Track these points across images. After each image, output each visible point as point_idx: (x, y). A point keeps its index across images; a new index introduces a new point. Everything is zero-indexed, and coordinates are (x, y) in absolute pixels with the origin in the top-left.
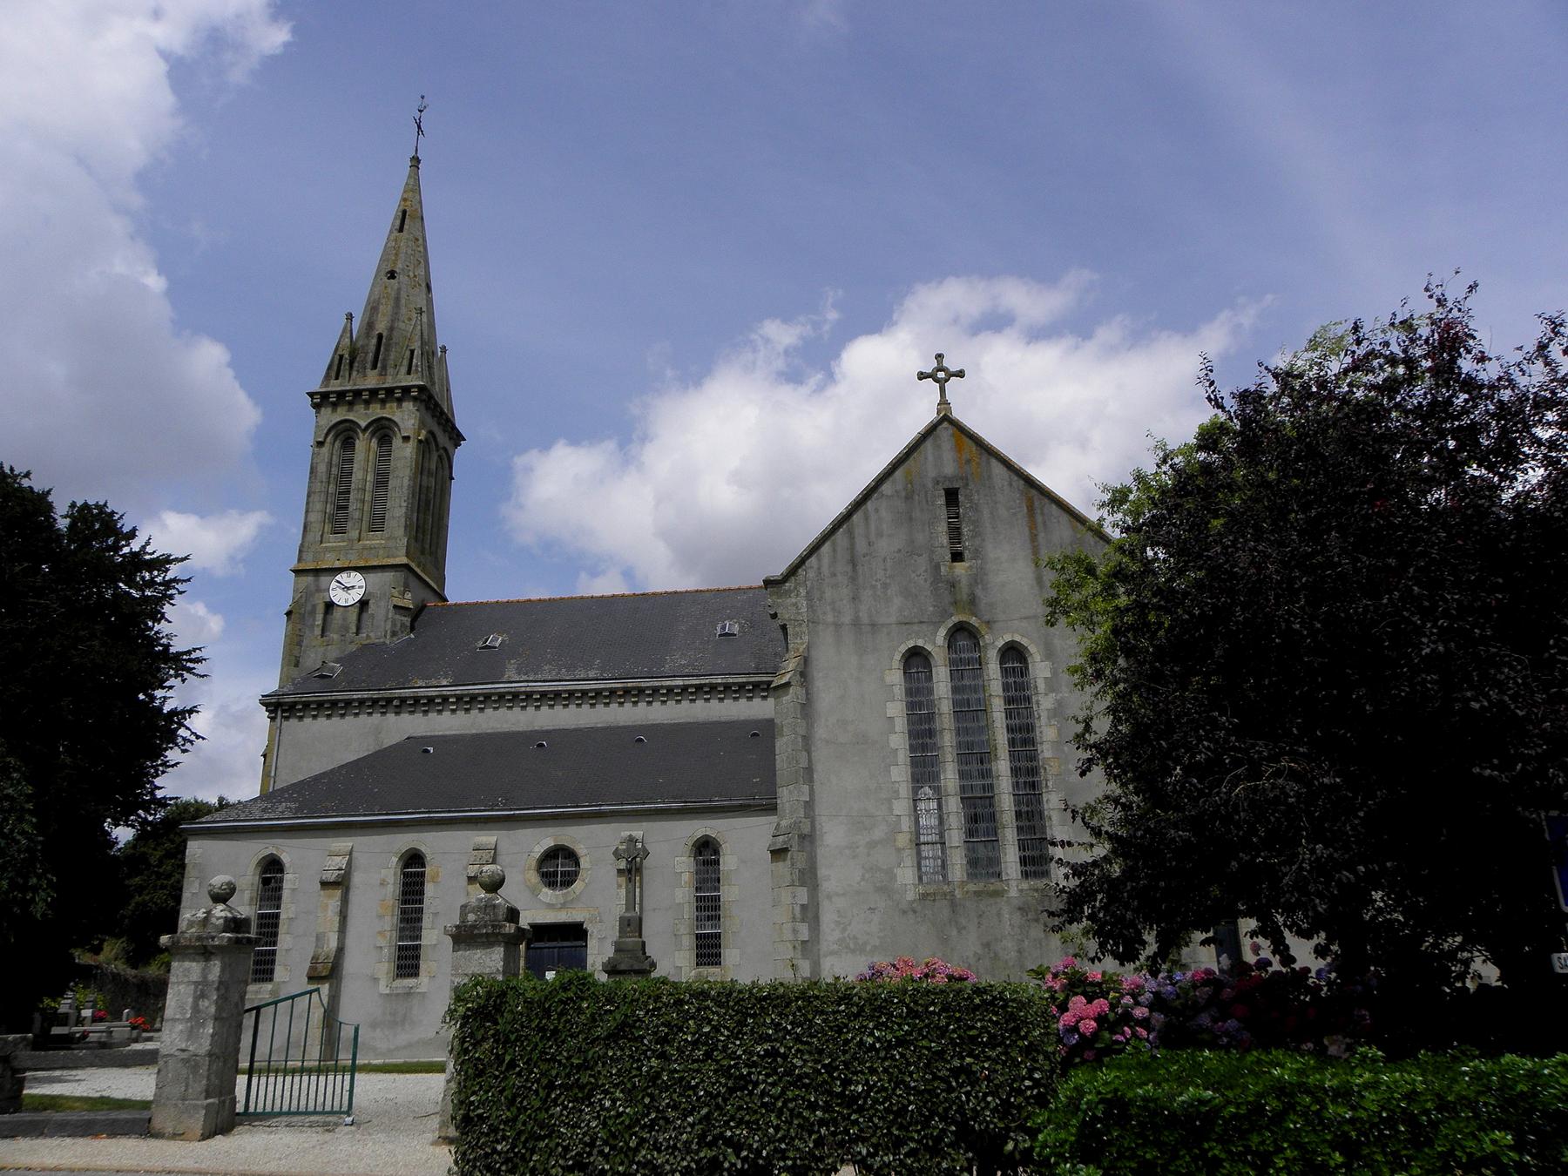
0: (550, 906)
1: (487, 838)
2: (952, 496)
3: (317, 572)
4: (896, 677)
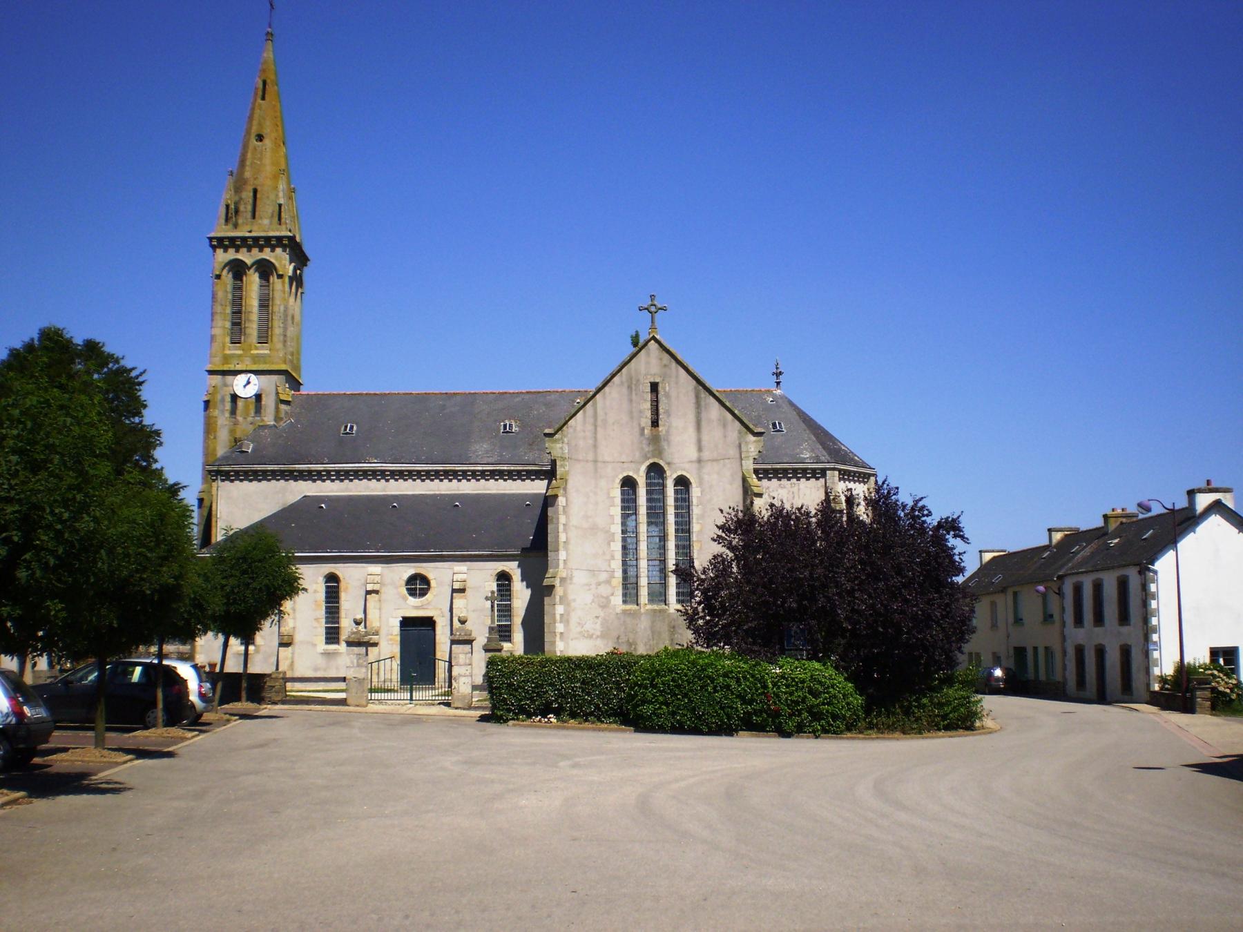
0: (417, 608)
1: (376, 569)
2: (654, 387)
3: (224, 373)
4: (617, 493)
